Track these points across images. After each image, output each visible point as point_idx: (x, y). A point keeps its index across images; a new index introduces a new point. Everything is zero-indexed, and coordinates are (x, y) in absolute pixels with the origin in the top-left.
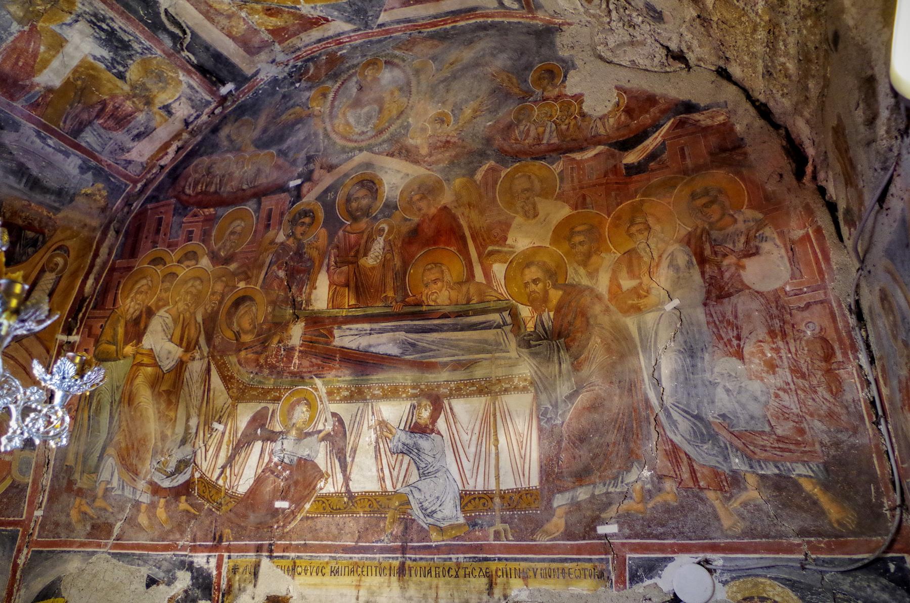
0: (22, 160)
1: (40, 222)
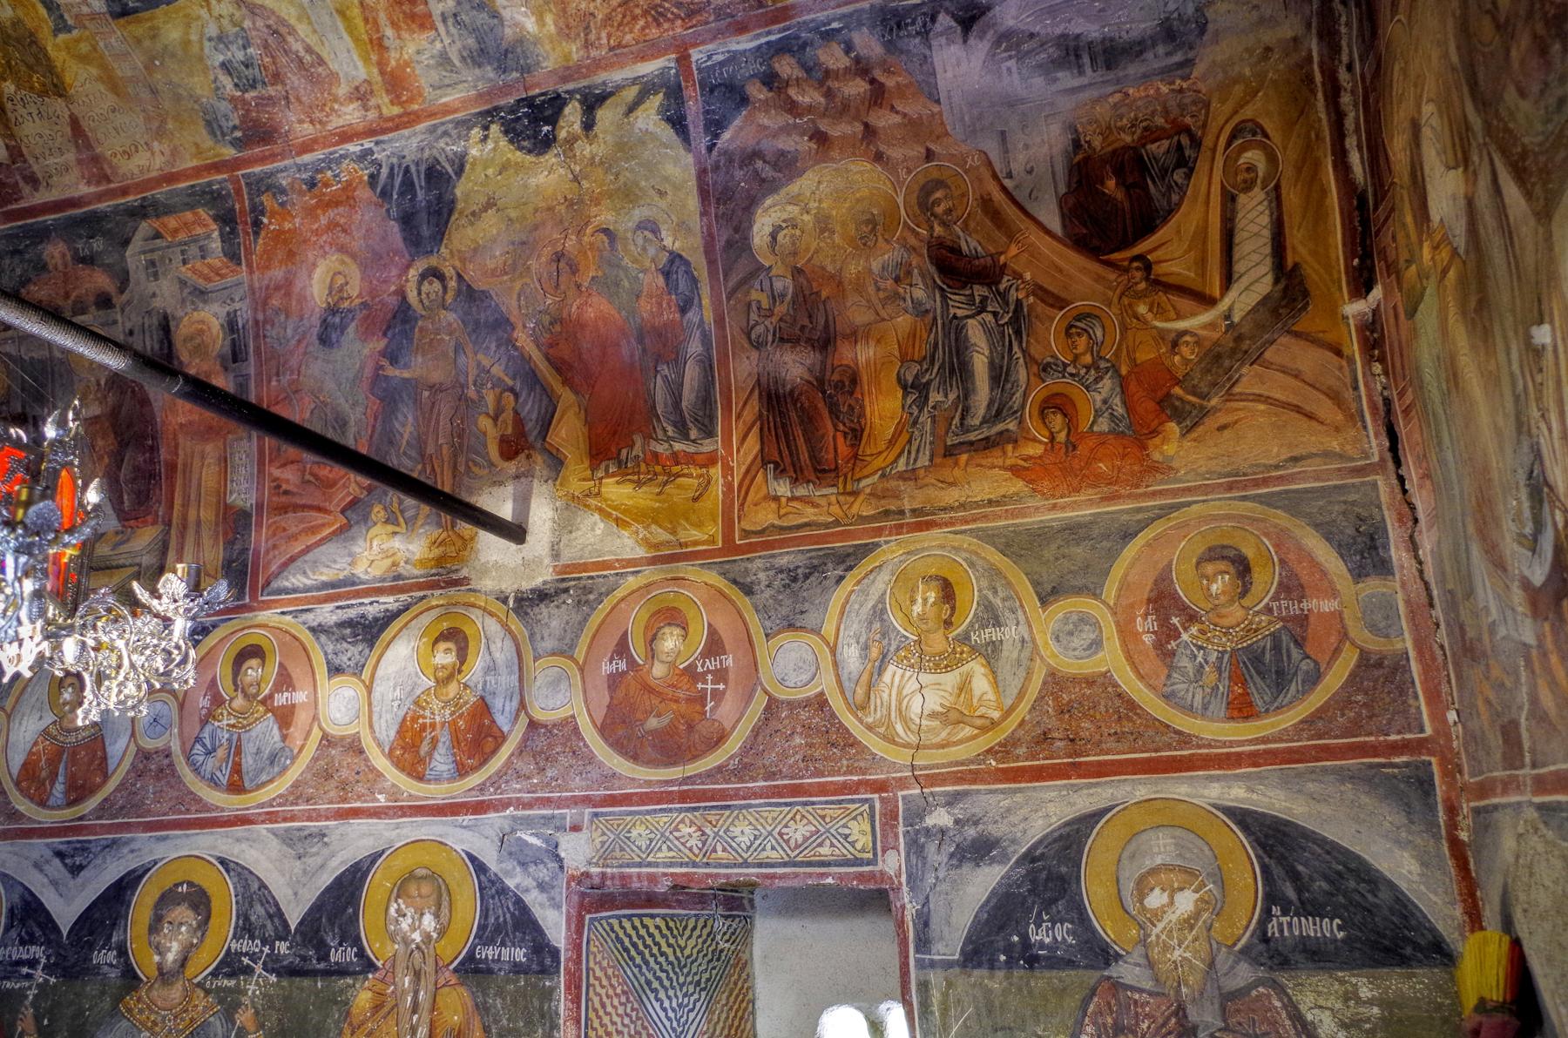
0: (1058, 31)
1: (1166, 112)
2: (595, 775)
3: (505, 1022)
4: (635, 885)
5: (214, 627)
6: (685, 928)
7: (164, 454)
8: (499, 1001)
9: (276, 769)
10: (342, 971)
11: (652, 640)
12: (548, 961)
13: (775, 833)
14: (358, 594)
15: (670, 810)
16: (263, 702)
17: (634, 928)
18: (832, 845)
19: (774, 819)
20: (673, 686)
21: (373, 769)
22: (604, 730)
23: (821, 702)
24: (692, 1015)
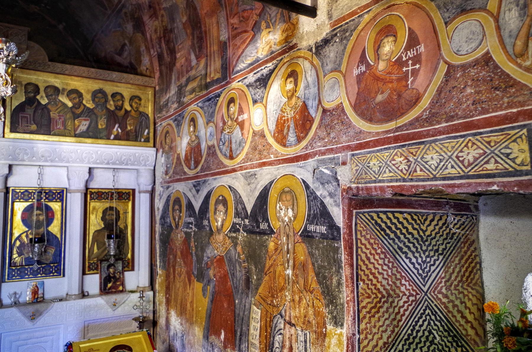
2: (352, 133)
3: (320, 262)
4: (374, 193)
5: (221, 93)
6: (426, 220)
7: (203, 29)
8: (317, 252)
9: (241, 148)
10: (263, 233)
11: (378, 47)
12: (335, 234)
13: (454, 157)
14: (260, 66)
15: (389, 148)
16: (236, 121)
17: (389, 218)
18: (496, 162)
19: (453, 147)
20: (390, 73)
21: (269, 144)
22: (356, 107)
23: (487, 59)
24: (433, 268)
